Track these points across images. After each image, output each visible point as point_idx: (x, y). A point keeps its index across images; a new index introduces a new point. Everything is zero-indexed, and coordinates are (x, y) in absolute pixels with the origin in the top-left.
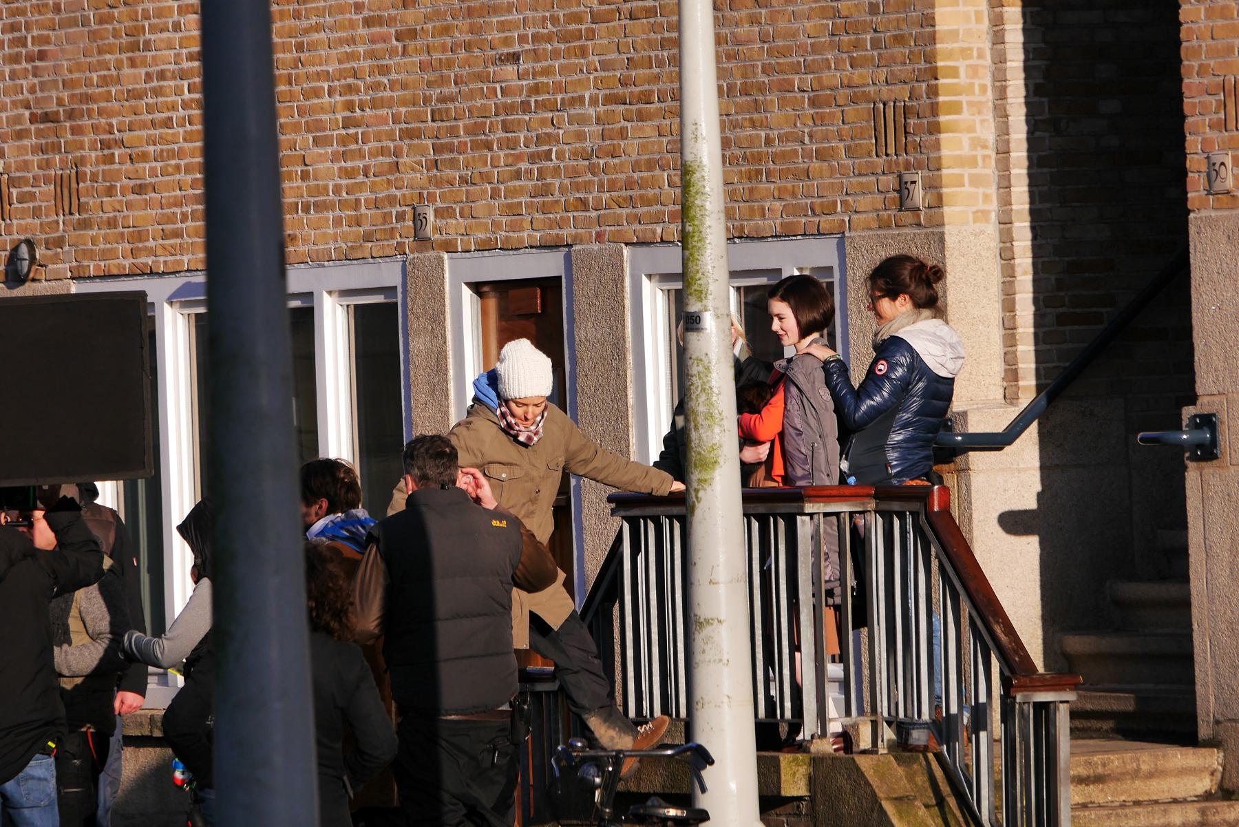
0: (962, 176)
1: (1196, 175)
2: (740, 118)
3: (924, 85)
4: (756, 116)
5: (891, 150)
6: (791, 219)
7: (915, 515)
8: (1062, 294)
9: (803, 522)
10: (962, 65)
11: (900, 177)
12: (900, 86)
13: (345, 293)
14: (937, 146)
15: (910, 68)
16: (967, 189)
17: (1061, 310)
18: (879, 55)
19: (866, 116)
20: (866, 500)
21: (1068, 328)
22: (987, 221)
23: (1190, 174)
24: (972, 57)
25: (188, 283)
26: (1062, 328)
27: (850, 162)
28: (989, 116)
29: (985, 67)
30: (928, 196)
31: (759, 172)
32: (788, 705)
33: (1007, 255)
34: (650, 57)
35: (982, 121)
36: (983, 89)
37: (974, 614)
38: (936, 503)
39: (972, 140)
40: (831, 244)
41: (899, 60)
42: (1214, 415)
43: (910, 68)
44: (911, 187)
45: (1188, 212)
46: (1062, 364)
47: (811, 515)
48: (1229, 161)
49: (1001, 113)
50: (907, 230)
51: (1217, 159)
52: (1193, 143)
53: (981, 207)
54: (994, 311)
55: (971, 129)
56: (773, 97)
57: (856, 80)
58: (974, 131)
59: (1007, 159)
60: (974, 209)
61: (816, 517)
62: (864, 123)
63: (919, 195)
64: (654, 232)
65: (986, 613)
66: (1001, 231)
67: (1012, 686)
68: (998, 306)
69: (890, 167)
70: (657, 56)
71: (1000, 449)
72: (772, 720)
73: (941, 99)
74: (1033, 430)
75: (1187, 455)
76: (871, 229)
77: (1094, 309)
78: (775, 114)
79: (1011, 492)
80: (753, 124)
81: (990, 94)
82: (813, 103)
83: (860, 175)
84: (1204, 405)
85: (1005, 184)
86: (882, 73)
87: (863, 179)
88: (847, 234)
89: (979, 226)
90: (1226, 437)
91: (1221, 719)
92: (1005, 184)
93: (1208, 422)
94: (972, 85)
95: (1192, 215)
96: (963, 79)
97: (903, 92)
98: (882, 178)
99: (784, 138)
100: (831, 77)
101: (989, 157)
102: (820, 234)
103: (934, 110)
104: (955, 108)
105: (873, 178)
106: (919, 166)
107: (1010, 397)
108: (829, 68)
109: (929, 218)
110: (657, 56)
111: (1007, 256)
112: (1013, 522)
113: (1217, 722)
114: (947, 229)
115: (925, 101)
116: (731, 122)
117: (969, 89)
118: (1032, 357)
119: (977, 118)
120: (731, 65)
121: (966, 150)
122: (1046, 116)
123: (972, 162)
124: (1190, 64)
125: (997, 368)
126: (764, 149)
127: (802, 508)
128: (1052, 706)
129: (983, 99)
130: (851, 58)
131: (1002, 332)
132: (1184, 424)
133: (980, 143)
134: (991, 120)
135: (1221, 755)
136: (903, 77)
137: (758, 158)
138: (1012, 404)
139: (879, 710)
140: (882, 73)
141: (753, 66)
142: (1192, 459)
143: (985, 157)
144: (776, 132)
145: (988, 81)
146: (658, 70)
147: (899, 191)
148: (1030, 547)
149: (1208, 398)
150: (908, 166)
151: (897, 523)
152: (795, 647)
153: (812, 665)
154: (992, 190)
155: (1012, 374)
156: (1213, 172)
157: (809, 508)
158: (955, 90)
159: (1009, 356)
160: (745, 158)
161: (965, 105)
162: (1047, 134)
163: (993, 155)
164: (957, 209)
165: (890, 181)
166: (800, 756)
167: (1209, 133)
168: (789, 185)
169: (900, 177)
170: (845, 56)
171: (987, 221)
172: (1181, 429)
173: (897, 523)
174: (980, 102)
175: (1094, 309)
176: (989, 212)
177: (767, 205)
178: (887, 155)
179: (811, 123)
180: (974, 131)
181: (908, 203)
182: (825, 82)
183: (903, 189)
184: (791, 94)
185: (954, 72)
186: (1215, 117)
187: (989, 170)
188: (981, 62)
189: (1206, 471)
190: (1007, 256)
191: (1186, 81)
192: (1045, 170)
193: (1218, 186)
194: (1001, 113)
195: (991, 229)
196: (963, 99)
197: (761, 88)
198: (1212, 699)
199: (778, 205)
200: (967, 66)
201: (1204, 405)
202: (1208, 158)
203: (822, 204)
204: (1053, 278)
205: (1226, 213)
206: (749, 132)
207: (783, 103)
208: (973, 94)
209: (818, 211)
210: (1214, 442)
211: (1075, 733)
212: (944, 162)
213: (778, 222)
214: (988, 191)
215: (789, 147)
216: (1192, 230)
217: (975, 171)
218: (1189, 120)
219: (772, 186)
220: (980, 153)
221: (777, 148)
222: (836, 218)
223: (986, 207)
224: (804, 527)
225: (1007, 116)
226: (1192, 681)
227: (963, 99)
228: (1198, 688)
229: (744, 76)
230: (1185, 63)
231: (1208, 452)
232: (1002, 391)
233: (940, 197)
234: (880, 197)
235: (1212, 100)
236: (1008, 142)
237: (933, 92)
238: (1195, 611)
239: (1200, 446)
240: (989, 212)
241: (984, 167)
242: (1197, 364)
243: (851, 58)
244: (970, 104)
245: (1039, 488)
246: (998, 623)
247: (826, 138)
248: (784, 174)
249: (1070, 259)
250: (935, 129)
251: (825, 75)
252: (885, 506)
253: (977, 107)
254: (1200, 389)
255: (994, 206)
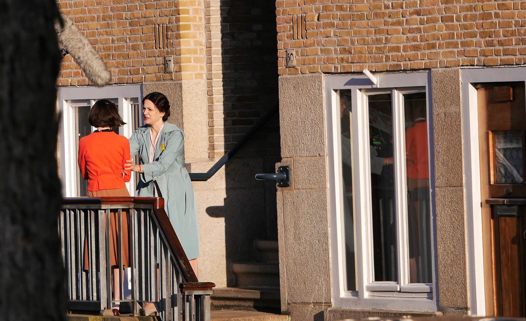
0: (190, 58)
1: (282, 59)
2: (102, 31)
3: (174, 17)
4: (108, 30)
5: (161, 46)
6: (122, 76)
7: (150, 210)
8: (235, 111)
9: (101, 213)
10: (191, 8)
11: (165, 58)
12: (165, 17)
13: (74, 101)
14: (179, 44)
15: (169, 9)
16: (193, 64)
17: (234, 118)
18: (157, 3)
19: (151, 31)
20: (130, 203)
21: (237, 126)
22: (202, 78)
23: (279, 59)
24: (196, 5)
25: (353, 79)
26: (235, 126)
27: (145, 51)
28: (203, 31)
29: (201, 9)
30: (176, 67)
31: (109, 55)
32: (95, 294)
33: (210, 93)
34: (66, 3)
35: (200, 33)
36: (200, 19)
37: (172, 255)
38: (158, 205)
39: (195, 41)
40: (424, 75)
41: (165, 6)
42: (288, 167)
43: (169, 9)
44: (169, 63)
45: (278, 75)
46: (234, 142)
47: (105, 210)
48: (294, 53)
49: (208, 30)
50: (167, 82)
51: (290, 52)
52: (280, 45)
53: (199, 72)
54: (205, 119)
55: (195, 37)
56: (115, 22)
57: (148, 15)
58: (196, 38)
59: (210, 51)
60: (196, 73)
61: (107, 211)
62: (151, 34)
63: (172, 66)
64: (68, 81)
65: (177, 255)
66: (208, 82)
67: (183, 288)
68: (206, 116)
69: (161, 54)
70: (69, 3)
71: (206, 180)
72: (78, 301)
73: (181, 23)
74: (222, 170)
75: (277, 184)
76: (153, 81)
77: (249, 118)
78: (116, 29)
79: (210, 199)
80: (107, 33)
81: (203, 21)
82: (131, 24)
83: (149, 57)
84: (284, 162)
85: (210, 62)
86: (158, 12)
87: (150, 59)
88: (144, 83)
89: (198, 80)
90: (292, 177)
91: (290, 302)
92: (210, 62)
93: (285, 170)
94: (195, 17)
95: (280, 77)
96: (191, 15)
97: (166, 20)
98: (157, 58)
99: (119, 40)
100: (138, 13)
101: (203, 49)
102: (133, 83)
103: (178, 28)
104: (187, 27)
105: (154, 58)
106: (172, 53)
107: (211, 157)
108: (137, 9)
109: (176, 77)
110: (69, 3)
111: (210, 94)
112: (213, 212)
113: (289, 304)
114: (183, 82)
115: (175, 24)
116: (98, 32)
117: (194, 19)
118: (222, 139)
119: (198, 32)
120: (98, 7)
121: (192, 47)
122: (228, 31)
123: (195, 52)
124: (279, 9)
125: (206, 144)
126: (111, 45)
127: (100, 207)
128: (202, 297)
129: (200, 24)
130: (146, 5)
131: (208, 128)
132: (276, 171)
133: (197, 43)
134: (204, 33)
135: (290, 318)
136: (166, 13)
137: (109, 49)
138: (212, 160)
139: (135, 297)
140: (158, 12)
141: (107, 8)
142: (280, 186)
143: (201, 50)
144: (116, 37)
145: (203, 15)
146: (70, 9)
147: (164, 65)
148: (221, 222)
149: (286, 159)
150: (168, 53)
151: (142, 214)
152: (98, 270)
153: (105, 277)
154: (204, 65)
155: (212, 147)
156: (288, 58)
157: (104, 207)
158: (187, 19)
159: (211, 139)
160: (104, 49)
161: (192, 26)
162: (228, 39)
163: (205, 48)
164: (188, 73)
165: (160, 60)
166: (98, 317)
167: (288, 41)
168: (121, 61)
169: (165, 58)
170: (143, 4)
171: (202, 78)
172: (275, 172)
173: (142, 214)
174: (199, 25)
175: (249, 118)
176: (203, 74)
177: (112, 70)
178: (160, 48)
179: (130, 33)
180: (196, 38)
181: (168, 70)
182: (135, 16)
183: (166, 63)
184: (122, 20)
185: (187, 12)
186: (289, 33)
187: (203, 56)
188: (199, 7)
189: (285, 191)
190: (210, 94)
191: (278, 17)
192: (228, 56)
193: (290, 64)
194: (208, 30)
195: (204, 82)
196: (191, 23)
197: (110, 18)
198: (287, 293)
199: (117, 70)
200: (193, 9)
201: (284, 162)
202: (286, 51)
203: (134, 69)
204: (230, 104)
205: (293, 76)
206: (106, 37)
207: (119, 24)
208: (196, 21)
209: (132, 73)
210: (288, 178)
211: (214, 308)
212: (182, 52)
213: (117, 77)
214: (202, 65)
215: (121, 43)
216: (280, 84)
217: (196, 56)
218: (279, 34)
219: (114, 61)
220: (198, 47)
221: (116, 44)
222: (140, 76)
223: (202, 72)
224: (102, 215)
225: (210, 31)
226: (278, 285)
227: (191, 23)
228: (281, 288)
229: (104, 12)
230: (277, 9)
231: (285, 183)
232: (208, 154)
233: (180, 67)
234: (157, 67)
235: (288, 25)
236: (211, 43)
237: (178, 20)
238: (280, 254)
239: (282, 180)
240: (203, 74)
241: (200, 54)
242: (281, 144)
243: (146, 5)
244: (195, 26)
245: (225, 196)
246: (182, 259)
247: (136, 40)
248: (119, 56)
249: (239, 95)
250: (178, 37)
251: (135, 12)
252: (137, 206)
253: (197, 27)
254: (282, 156)
255: (205, 72)
